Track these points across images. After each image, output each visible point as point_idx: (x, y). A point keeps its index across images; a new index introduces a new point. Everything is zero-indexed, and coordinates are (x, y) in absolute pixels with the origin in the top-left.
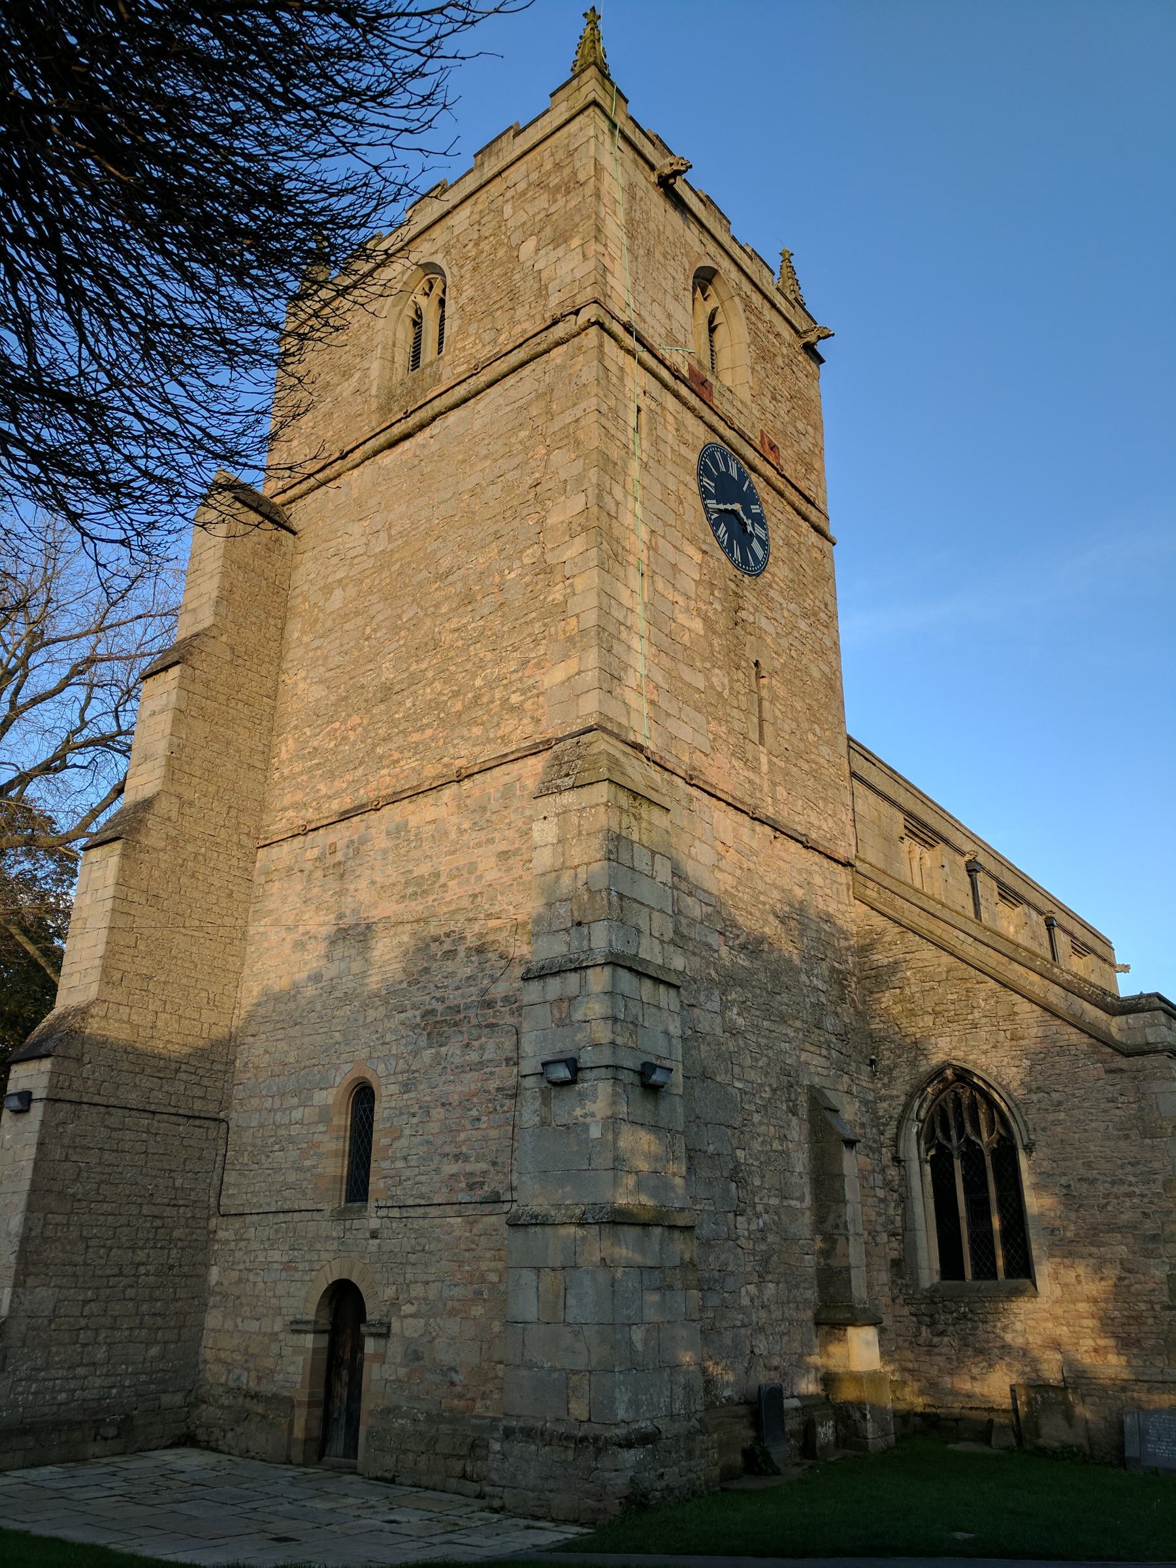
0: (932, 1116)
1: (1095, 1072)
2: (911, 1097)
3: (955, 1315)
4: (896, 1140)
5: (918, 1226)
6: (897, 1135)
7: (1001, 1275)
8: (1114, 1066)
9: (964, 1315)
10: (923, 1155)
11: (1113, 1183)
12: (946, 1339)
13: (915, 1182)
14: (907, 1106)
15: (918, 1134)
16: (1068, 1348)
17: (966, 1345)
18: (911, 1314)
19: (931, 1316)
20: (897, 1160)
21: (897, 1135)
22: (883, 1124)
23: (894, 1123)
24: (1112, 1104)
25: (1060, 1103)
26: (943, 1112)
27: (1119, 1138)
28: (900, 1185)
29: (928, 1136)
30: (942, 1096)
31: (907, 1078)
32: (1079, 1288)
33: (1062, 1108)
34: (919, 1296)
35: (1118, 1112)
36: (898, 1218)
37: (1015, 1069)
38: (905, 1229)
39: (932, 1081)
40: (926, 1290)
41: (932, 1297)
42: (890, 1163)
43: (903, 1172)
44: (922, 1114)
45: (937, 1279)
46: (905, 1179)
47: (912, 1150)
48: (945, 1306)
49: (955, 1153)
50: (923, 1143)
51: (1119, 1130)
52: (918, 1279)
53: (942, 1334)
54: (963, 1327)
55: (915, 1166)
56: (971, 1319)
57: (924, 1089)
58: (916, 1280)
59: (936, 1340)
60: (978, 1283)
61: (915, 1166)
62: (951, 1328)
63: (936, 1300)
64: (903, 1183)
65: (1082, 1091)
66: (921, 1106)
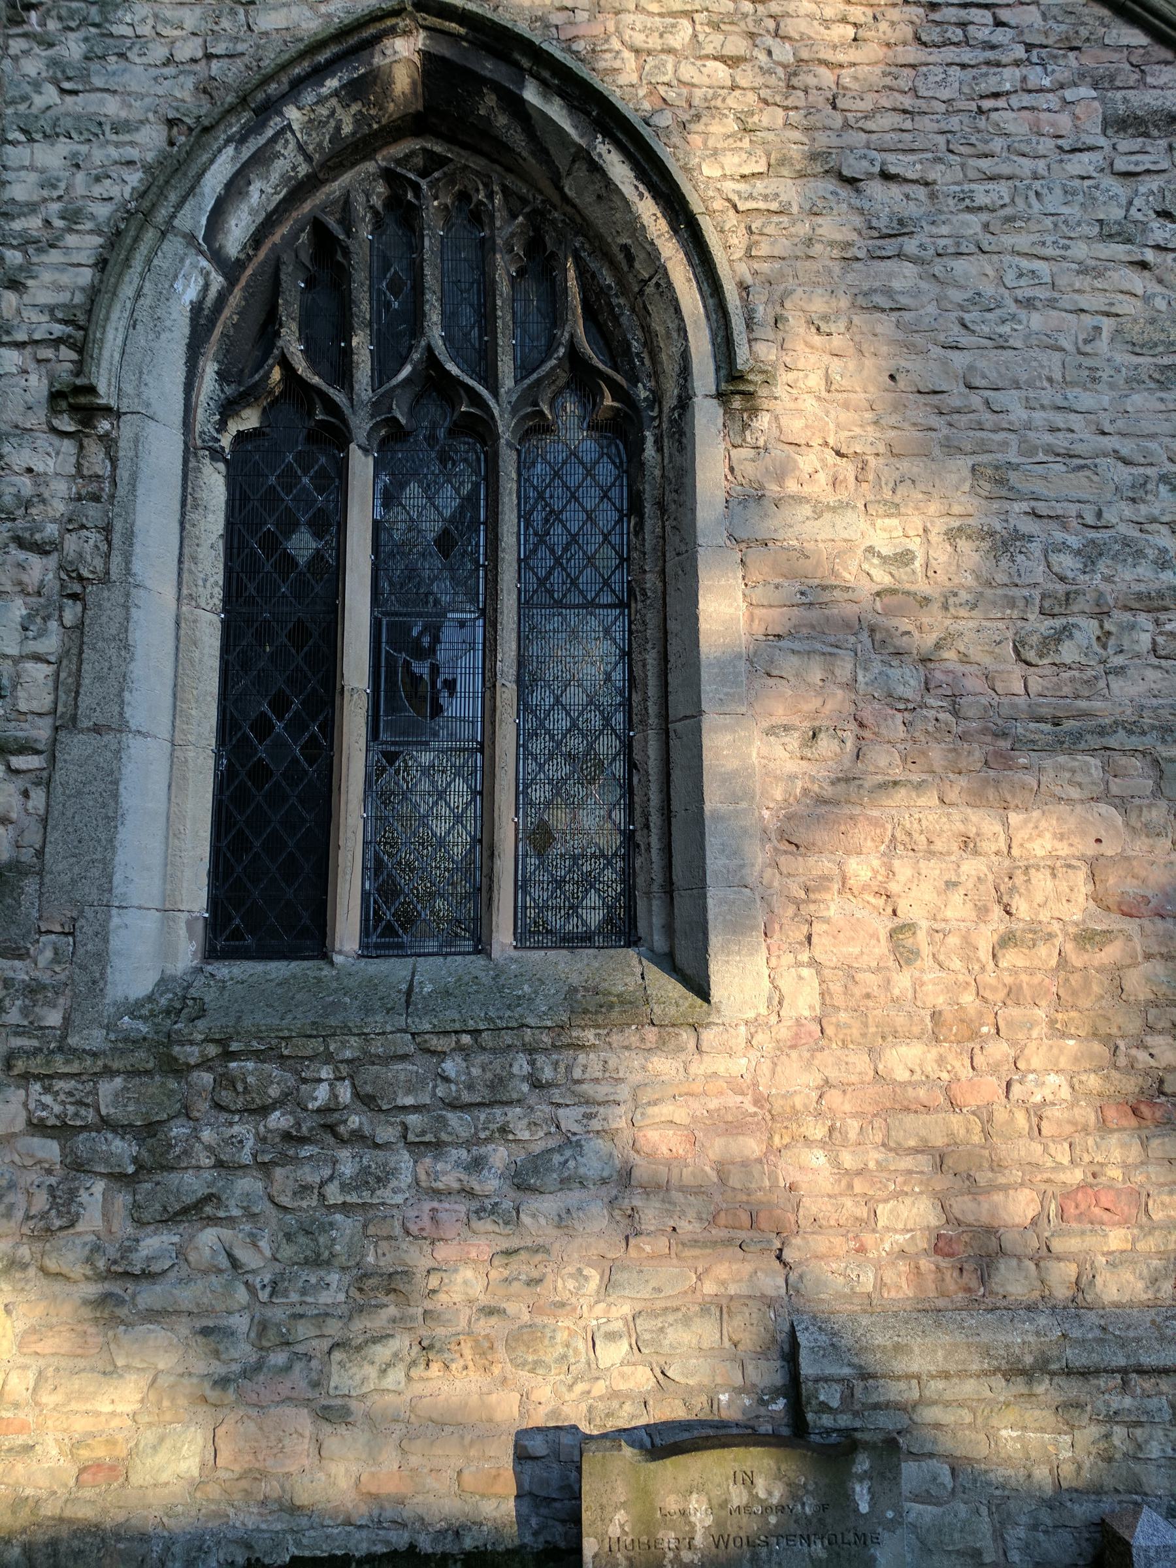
0: (275, 268)
1: (1064, 121)
2: (190, 138)
3: (278, 1120)
4: (80, 328)
5: (136, 717)
6: (96, 297)
7: (503, 935)
8: (1144, 100)
9: (329, 1124)
10: (204, 419)
11: (1090, 555)
12: (209, 1237)
13: (154, 514)
14: (173, 172)
15: (202, 321)
16: (820, 1243)
17: (316, 1262)
18: (38, 1127)
19: (149, 1130)
20: (78, 406)
21: (96, 297)
22: (26, 243)
23: (84, 245)
24: (1119, 250)
25: (902, 228)
26: (327, 248)
27: (1134, 382)
28: (72, 524)
29: (239, 340)
30: (335, 188)
31: (189, 49)
32: (903, 981)
33: (911, 246)
34: (96, 1038)
35: (1137, 282)
36: (39, 672)
37: (721, 72)
38: (65, 722)
39: (318, 74)
40: (133, 1009)
41: (164, 1041)
42: (37, 419)
43: (97, 461)
44: (236, 233)
45: (187, 951)
46: (102, 497)
47: (158, 378)
48: (227, 1081)
49: (361, 425)
50: (209, 369)
51: (1135, 349)
52: (101, 958)
53: (196, 1211)
54: (310, 1176)
55: (158, 449)
56: (358, 1137)
57: (268, 109)
58: (88, 962)
59: (155, 1244)
60: (393, 970)
61: (158, 449)
62: (248, 1184)
63: (191, 1054)
64: (93, 511)
65: (1003, 188)
66: (235, 188)
